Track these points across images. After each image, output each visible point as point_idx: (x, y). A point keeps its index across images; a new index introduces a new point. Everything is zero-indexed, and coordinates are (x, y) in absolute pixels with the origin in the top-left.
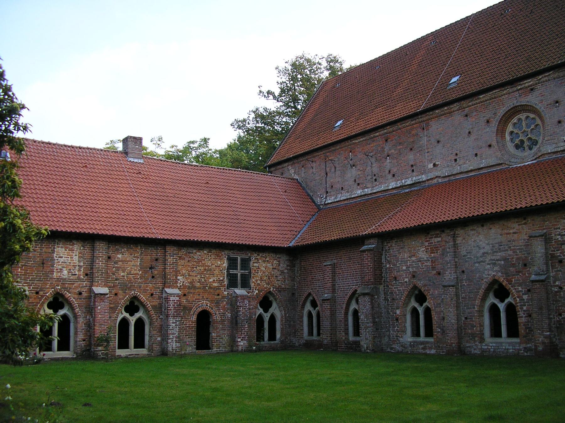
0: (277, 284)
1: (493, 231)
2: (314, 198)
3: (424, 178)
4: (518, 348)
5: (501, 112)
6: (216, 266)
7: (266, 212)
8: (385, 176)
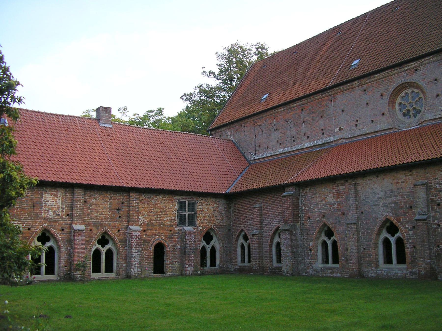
0: (217, 222)
1: (386, 181)
2: (245, 155)
3: (332, 139)
4: (406, 272)
5: (392, 87)
6: (169, 208)
7: (208, 166)
8: (301, 138)
